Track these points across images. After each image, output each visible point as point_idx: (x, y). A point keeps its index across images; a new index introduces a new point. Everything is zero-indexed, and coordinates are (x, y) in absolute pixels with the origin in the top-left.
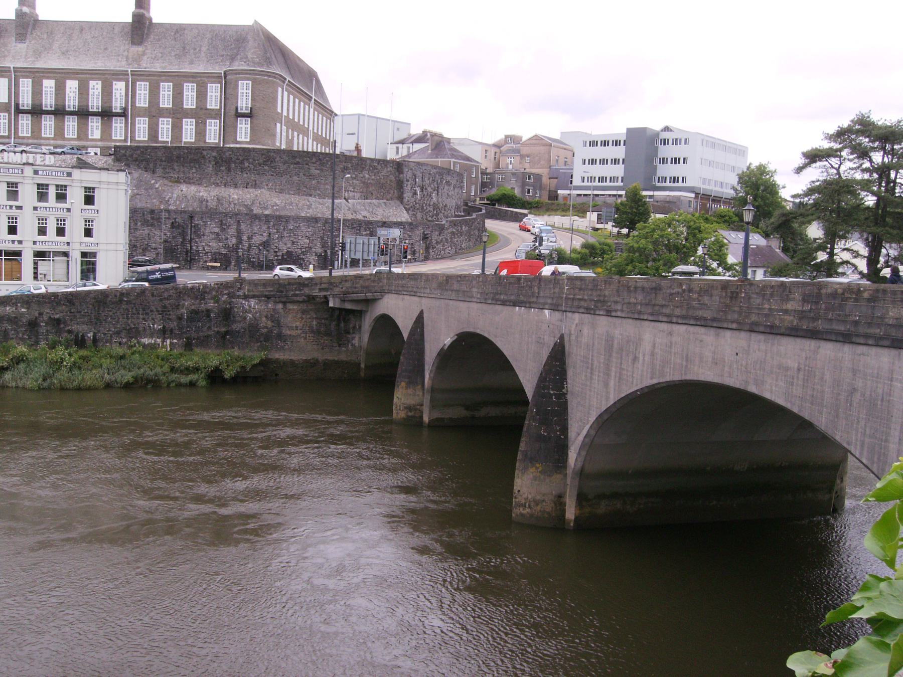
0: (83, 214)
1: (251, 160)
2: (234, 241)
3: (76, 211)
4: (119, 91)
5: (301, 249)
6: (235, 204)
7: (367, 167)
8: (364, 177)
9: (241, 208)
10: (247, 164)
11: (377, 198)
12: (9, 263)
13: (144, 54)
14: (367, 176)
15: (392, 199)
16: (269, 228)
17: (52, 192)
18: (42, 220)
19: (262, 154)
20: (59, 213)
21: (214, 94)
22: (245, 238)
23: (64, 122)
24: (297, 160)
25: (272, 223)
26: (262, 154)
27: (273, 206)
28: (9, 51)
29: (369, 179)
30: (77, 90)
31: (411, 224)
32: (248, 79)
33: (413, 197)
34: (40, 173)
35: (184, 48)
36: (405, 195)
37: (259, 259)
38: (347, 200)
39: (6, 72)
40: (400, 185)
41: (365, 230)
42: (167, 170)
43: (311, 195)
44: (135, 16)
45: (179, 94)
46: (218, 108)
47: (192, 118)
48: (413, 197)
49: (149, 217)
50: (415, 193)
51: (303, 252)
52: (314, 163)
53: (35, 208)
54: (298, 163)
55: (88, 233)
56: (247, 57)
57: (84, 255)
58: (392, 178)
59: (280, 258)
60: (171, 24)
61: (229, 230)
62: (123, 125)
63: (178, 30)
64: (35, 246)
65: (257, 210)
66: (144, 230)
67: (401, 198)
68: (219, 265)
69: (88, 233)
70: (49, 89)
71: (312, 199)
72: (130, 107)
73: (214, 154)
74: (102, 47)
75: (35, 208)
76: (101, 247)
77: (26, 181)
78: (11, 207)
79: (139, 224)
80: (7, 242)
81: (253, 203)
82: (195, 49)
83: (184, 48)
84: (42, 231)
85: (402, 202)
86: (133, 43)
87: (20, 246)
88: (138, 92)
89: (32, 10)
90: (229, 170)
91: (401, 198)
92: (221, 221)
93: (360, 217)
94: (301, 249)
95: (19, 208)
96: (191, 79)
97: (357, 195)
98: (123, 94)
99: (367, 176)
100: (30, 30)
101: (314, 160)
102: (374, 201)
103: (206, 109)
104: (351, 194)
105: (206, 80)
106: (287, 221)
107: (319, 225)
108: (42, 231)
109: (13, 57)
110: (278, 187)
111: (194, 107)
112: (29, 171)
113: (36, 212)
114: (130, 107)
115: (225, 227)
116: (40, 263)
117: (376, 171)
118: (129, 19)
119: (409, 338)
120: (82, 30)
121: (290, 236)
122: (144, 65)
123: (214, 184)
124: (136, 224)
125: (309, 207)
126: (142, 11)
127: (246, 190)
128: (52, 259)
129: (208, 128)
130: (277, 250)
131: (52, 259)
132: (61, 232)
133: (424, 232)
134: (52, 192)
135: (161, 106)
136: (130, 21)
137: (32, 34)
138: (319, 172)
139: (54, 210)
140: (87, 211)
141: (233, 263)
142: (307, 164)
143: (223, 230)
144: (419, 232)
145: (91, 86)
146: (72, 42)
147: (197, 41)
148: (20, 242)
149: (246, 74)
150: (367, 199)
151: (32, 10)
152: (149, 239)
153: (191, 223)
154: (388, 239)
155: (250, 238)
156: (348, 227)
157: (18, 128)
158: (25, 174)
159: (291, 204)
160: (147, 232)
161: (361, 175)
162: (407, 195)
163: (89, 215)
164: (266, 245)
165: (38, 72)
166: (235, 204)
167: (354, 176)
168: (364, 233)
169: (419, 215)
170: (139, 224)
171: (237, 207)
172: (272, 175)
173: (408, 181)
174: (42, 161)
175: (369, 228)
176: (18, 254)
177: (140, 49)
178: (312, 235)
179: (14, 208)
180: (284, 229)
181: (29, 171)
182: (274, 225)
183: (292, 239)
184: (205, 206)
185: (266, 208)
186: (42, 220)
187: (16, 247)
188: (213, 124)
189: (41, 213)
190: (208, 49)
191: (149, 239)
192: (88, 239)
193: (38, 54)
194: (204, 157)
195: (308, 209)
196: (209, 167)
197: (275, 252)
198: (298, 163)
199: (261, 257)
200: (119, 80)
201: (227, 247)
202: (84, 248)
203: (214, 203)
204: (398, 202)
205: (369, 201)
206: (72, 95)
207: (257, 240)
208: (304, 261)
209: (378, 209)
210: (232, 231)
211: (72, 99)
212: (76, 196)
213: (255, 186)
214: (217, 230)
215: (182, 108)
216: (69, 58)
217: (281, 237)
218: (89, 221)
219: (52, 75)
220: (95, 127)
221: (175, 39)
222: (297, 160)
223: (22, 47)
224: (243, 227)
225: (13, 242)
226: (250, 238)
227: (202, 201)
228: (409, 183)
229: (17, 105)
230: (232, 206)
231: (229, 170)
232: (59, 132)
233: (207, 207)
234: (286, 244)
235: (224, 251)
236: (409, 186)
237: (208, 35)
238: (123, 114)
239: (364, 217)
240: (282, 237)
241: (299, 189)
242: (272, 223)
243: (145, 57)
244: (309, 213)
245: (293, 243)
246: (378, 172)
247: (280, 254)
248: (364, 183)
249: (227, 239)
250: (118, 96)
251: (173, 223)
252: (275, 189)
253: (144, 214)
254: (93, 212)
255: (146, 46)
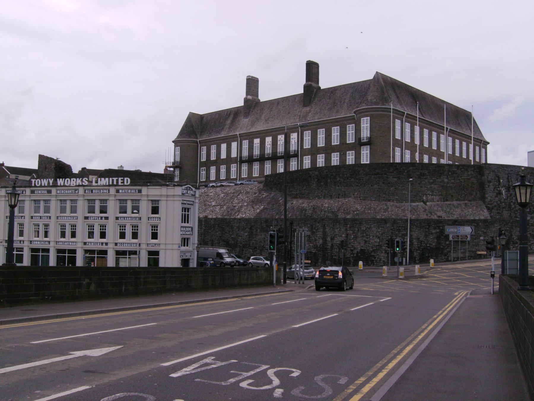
0: (149, 221)
1: (341, 175)
2: (321, 241)
3: (144, 220)
4: (294, 140)
5: (372, 248)
6: (325, 211)
7: (446, 172)
8: (443, 181)
9: (329, 215)
10: (338, 179)
11: (458, 200)
12: (100, 259)
13: (310, 111)
14: (446, 180)
15: (474, 200)
16: (346, 230)
17: (129, 205)
18: (123, 227)
19: (349, 169)
20: (132, 221)
21: (351, 132)
22: (329, 239)
23: (264, 165)
24: (377, 171)
25: (349, 226)
26: (349, 169)
27: (354, 212)
28: (239, 125)
29: (448, 183)
30: (271, 143)
31: (485, 221)
32: (367, 116)
33: (496, 197)
34: (121, 191)
35: (334, 103)
36: (487, 196)
37: (339, 256)
38: (425, 203)
39: (234, 138)
40: (482, 187)
41: (435, 228)
42: (291, 190)
43: (389, 200)
44: (306, 87)
45: (329, 135)
46: (406, 150)
47: (337, 152)
48: (496, 197)
49: (264, 225)
50: (500, 193)
51: (374, 251)
52: (391, 173)
53: (32, 217)
54: (378, 174)
55: (155, 236)
56: (367, 100)
57: (150, 253)
58: (474, 180)
59: (355, 255)
60: (328, 88)
61: (318, 233)
62: (296, 163)
63: (333, 91)
64: (116, 247)
65: (341, 216)
66: (261, 235)
67: (483, 199)
68: (310, 262)
69: (155, 236)
70: (257, 145)
71: (390, 204)
72: (300, 150)
73: (317, 173)
74: (287, 112)
75: (117, 218)
76: (162, 247)
77: (142, 198)
78: (102, 218)
79: (259, 230)
80: (98, 244)
81: (339, 210)
82: (341, 102)
83: (334, 103)
84: (123, 235)
85: (484, 202)
86: (304, 106)
87: (106, 247)
88: (305, 138)
89: (255, 98)
90: (326, 184)
91: (483, 199)
92: (312, 226)
93: (435, 217)
94: (372, 248)
95: (107, 218)
96: (336, 124)
97: (436, 198)
98: (296, 141)
99: (446, 180)
100: (252, 110)
101: (391, 170)
102: (455, 203)
103: (346, 144)
104: (430, 197)
105: (346, 122)
106: (361, 224)
107: (388, 225)
108: (123, 235)
109: (241, 128)
110: (362, 195)
111: (338, 143)
112: (113, 190)
113: (117, 221)
114: (300, 150)
115: (314, 230)
116: (121, 259)
117: (455, 175)
118: (301, 91)
119: (170, 377)
120: (278, 104)
121: (363, 236)
122: (309, 119)
123: (317, 196)
124: (257, 231)
125: (386, 210)
126: (310, 83)
127: (337, 199)
128: (128, 256)
129: (347, 157)
130: (352, 249)
131: (128, 256)
132: (135, 235)
133: (500, 229)
134: (129, 205)
135: (354, 152)
136: (302, 92)
137: (253, 112)
138: (396, 179)
139: (130, 219)
140: (152, 219)
141: (320, 261)
142: (385, 174)
143: (313, 233)
144: (497, 227)
145: (279, 139)
146: (272, 112)
147: (343, 96)
148: (106, 244)
149: (366, 112)
150: (447, 200)
151: (255, 98)
152: (264, 242)
153: (291, 228)
154: (458, 236)
155: (332, 239)
156: (417, 226)
157: (241, 173)
158: (111, 193)
159: (370, 209)
160: (263, 236)
161: (439, 180)
162: (490, 195)
163: (154, 222)
164: (343, 245)
165: (251, 135)
166: (325, 211)
167: (431, 181)
168: (433, 231)
169: (506, 214)
170: (259, 230)
171: (326, 214)
172: (357, 186)
173: (490, 182)
174: (122, 183)
175: (439, 227)
176: (105, 252)
177: (308, 109)
178: (382, 234)
179: (103, 219)
180: (358, 231)
181: (113, 190)
182: (350, 227)
183: (364, 239)
184: (304, 214)
185: (348, 214)
186: (123, 227)
187: (104, 247)
188: (351, 154)
189: (121, 222)
190: (349, 101)
191: (264, 242)
192: (154, 241)
193: (253, 124)
194: (310, 176)
195: (384, 212)
196: (313, 184)
197: (352, 250)
198: (378, 174)
199: (340, 255)
200: (294, 132)
201: (315, 247)
202: (150, 248)
203: (310, 212)
204: (480, 202)
205: (449, 202)
206: (269, 146)
207: (337, 240)
208: (375, 258)
209: (456, 210)
210: (320, 234)
211: (268, 149)
212: (145, 207)
213: (345, 196)
214: (309, 233)
215: (331, 145)
216: (268, 123)
217: (356, 237)
218: (155, 227)
219: (258, 135)
220: (280, 167)
221: (330, 98)
222: (377, 171)
223: (246, 120)
224: (327, 230)
225: (102, 244)
226: (332, 239)
227: (303, 210)
228: (491, 184)
229: (241, 157)
230: (323, 213)
231: (326, 184)
232: (262, 170)
233: (305, 215)
234: (359, 243)
235: (314, 251)
236: (492, 187)
237: (351, 91)
238: (296, 155)
239: (439, 217)
240: (356, 238)
241: (379, 196)
242: (349, 226)
243: (310, 114)
244: (385, 215)
245: (366, 242)
246: (458, 176)
247: (355, 252)
248: (442, 186)
249: (316, 240)
250: (293, 143)
251: (279, 229)
252: (360, 197)
253: (261, 223)
254: (157, 219)
255: (312, 106)
